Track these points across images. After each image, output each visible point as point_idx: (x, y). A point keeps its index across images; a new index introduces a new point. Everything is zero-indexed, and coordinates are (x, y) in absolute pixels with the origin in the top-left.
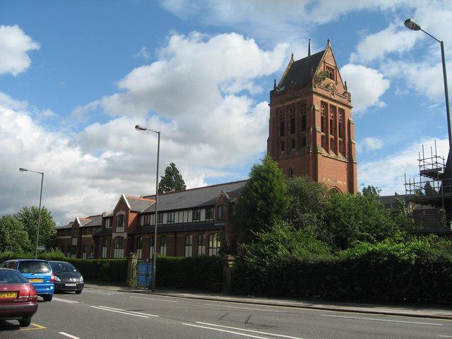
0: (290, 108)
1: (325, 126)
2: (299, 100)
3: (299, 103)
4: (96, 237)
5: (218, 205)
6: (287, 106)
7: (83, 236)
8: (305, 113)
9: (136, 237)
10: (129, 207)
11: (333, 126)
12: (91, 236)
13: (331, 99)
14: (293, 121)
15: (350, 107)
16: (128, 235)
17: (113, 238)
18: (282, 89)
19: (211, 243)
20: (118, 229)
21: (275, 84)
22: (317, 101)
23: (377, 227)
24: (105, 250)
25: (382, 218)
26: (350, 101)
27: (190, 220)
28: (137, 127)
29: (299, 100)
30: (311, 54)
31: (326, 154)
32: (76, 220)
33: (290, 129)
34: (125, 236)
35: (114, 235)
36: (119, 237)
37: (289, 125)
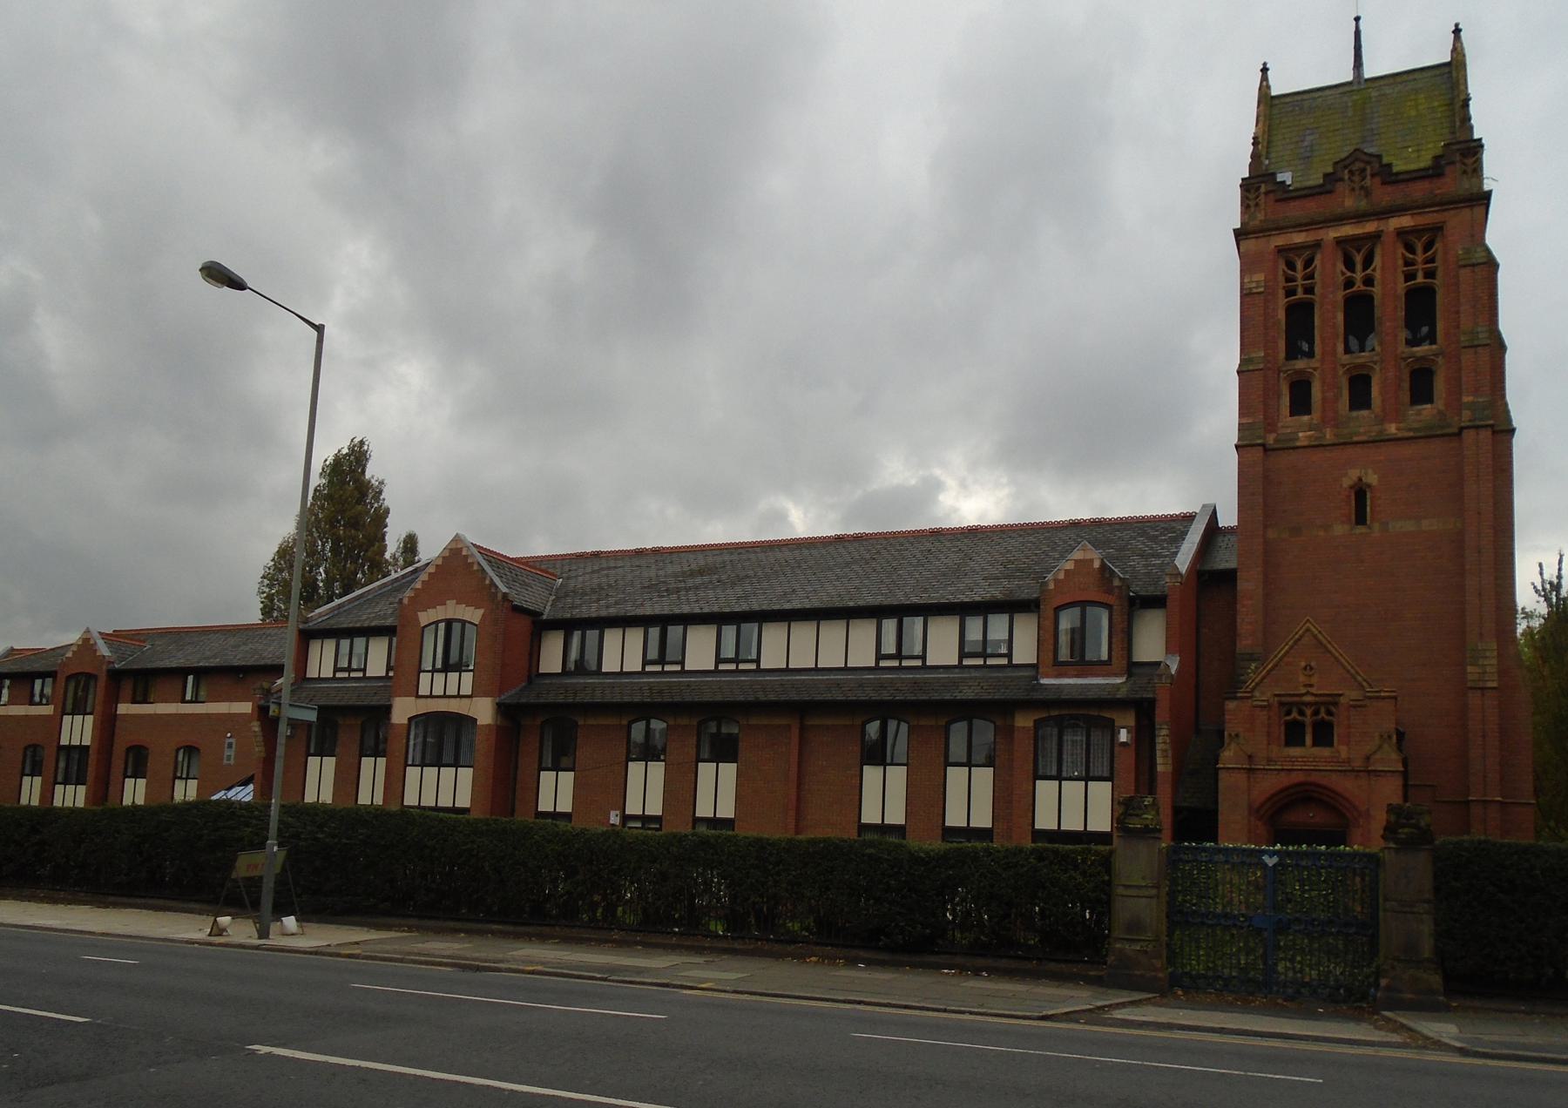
7: (124, 709)
16: (502, 709)
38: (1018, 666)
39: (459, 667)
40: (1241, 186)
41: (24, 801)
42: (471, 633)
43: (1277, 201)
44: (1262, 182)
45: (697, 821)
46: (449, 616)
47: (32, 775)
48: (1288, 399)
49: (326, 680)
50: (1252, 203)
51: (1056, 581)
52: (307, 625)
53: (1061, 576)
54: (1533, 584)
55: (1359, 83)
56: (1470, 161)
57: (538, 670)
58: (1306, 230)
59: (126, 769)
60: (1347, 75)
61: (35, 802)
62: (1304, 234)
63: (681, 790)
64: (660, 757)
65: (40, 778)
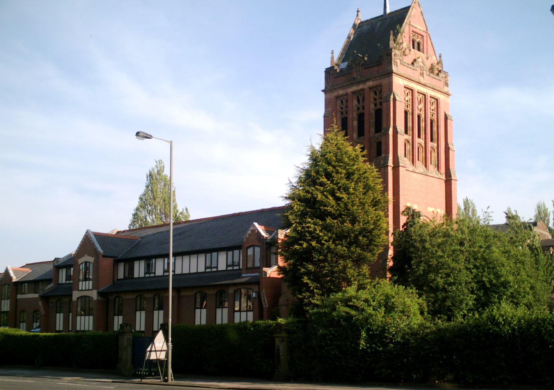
0: (360, 95)
1: (410, 124)
2: (370, 84)
3: (370, 88)
4: (45, 298)
5: (248, 245)
6: (353, 93)
7: (19, 296)
8: (381, 104)
9: (111, 298)
10: (100, 249)
11: (422, 124)
12: (36, 296)
13: (419, 83)
14: (361, 118)
15: (448, 94)
16: (100, 294)
17: (74, 298)
18: (344, 65)
19: (237, 304)
20: (82, 285)
21: (332, 58)
22: (398, 83)
23: (419, 327)
24: (60, 318)
25: (353, 293)
26: (447, 84)
27: (142, 275)
28: (137, 134)
29: (370, 84)
30: (388, 11)
31: (411, 168)
32: (7, 272)
33: (356, 129)
34: (94, 295)
35: (76, 295)
36: (86, 297)
37: (355, 123)
38: (220, 271)
39: (89, 279)
40: (325, 72)
41: (197, 323)
42: (91, 265)
43: (335, 77)
44: (331, 70)
45: (77, 331)
46: (86, 260)
47: (118, 315)
48: (382, 148)
49: (64, 284)
50: (328, 79)
51: (246, 238)
52: (58, 264)
53: (247, 236)
54: (505, 212)
55: (385, 15)
56: (389, 58)
57: (117, 277)
58: (343, 89)
59: (216, 305)
60: (382, 13)
61: (204, 322)
62: (342, 90)
63: (211, 317)
64: (423, 288)
65: (122, 316)
